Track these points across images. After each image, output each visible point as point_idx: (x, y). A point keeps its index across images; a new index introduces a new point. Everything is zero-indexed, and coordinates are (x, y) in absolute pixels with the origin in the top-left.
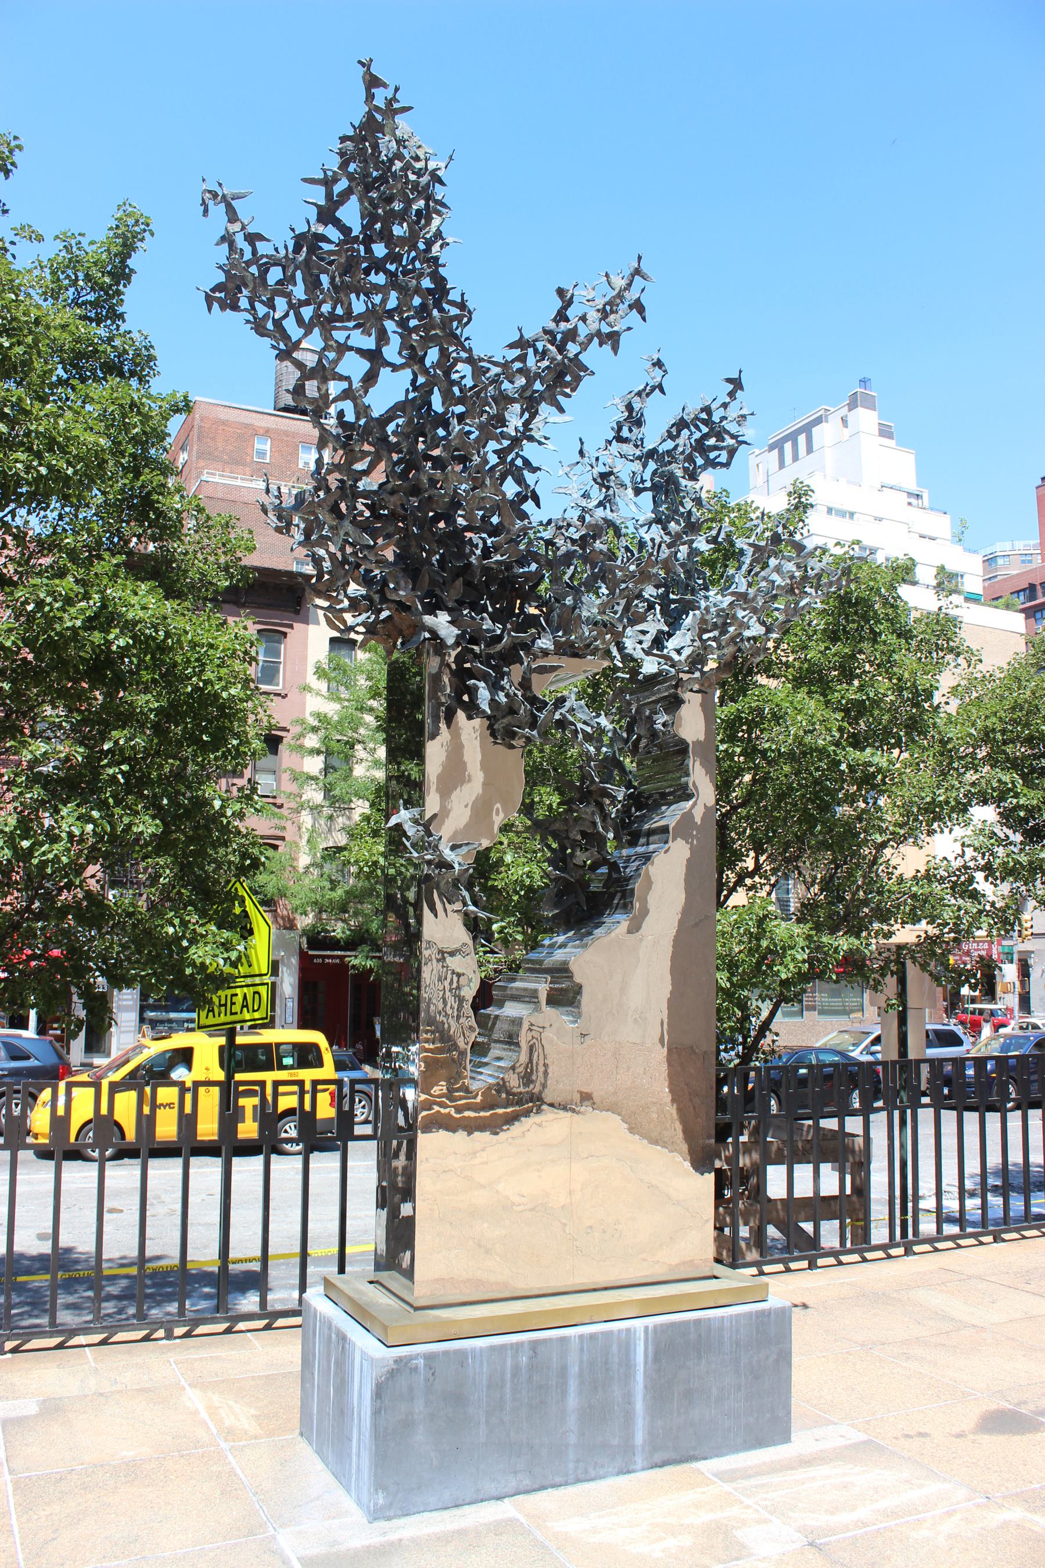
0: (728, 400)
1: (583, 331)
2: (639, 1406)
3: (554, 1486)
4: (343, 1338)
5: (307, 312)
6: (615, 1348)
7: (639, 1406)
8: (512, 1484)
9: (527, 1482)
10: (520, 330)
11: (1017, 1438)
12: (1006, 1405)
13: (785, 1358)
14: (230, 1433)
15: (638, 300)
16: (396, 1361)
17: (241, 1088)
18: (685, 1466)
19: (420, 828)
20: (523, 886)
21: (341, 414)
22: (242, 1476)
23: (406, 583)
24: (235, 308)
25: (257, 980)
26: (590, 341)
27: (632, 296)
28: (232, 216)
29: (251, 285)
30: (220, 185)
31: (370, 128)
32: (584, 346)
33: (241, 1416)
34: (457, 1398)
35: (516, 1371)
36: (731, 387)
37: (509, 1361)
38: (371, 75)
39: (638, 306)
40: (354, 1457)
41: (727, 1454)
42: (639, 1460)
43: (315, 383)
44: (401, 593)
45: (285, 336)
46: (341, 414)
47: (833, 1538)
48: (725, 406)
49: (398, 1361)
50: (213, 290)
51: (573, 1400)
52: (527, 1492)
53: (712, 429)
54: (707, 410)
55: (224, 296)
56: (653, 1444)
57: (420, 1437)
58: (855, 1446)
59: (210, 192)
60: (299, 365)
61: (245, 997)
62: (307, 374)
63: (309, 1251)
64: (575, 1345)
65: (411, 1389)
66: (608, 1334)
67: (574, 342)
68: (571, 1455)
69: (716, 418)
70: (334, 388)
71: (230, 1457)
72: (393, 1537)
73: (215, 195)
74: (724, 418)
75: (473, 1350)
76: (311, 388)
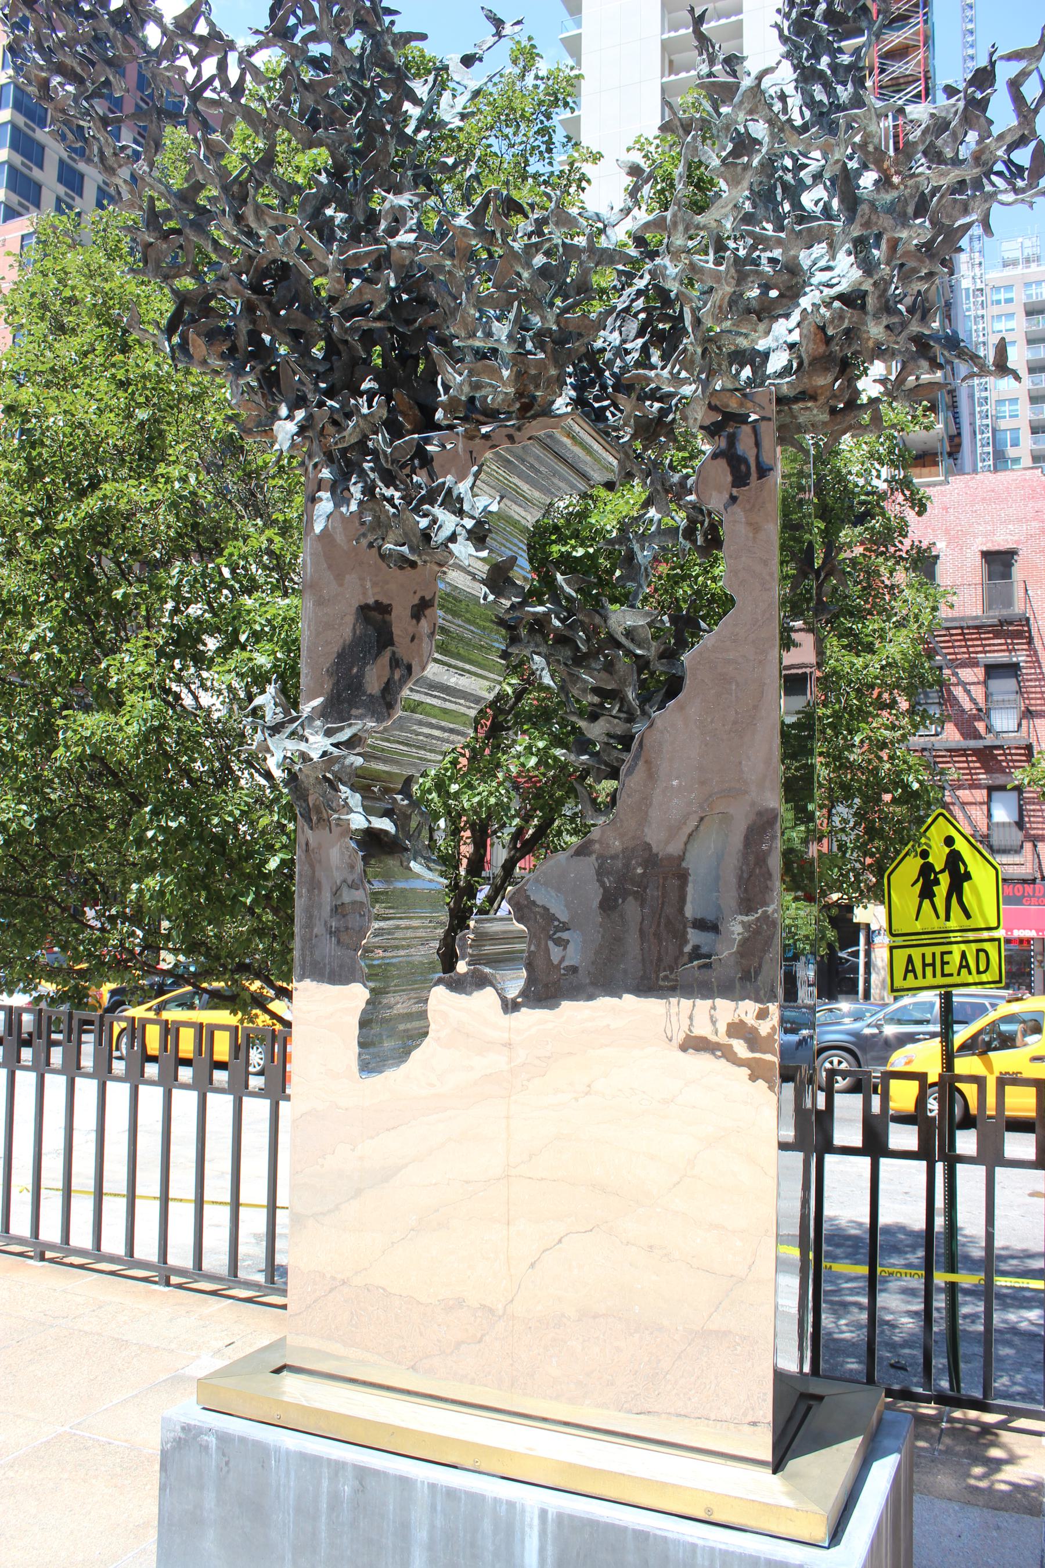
6: (487, 1526)
16: (183, 1428)
21: (687, 476)
25: (986, 935)
35: (335, 1501)
37: (325, 1483)
46: (687, 476)
61: (963, 955)
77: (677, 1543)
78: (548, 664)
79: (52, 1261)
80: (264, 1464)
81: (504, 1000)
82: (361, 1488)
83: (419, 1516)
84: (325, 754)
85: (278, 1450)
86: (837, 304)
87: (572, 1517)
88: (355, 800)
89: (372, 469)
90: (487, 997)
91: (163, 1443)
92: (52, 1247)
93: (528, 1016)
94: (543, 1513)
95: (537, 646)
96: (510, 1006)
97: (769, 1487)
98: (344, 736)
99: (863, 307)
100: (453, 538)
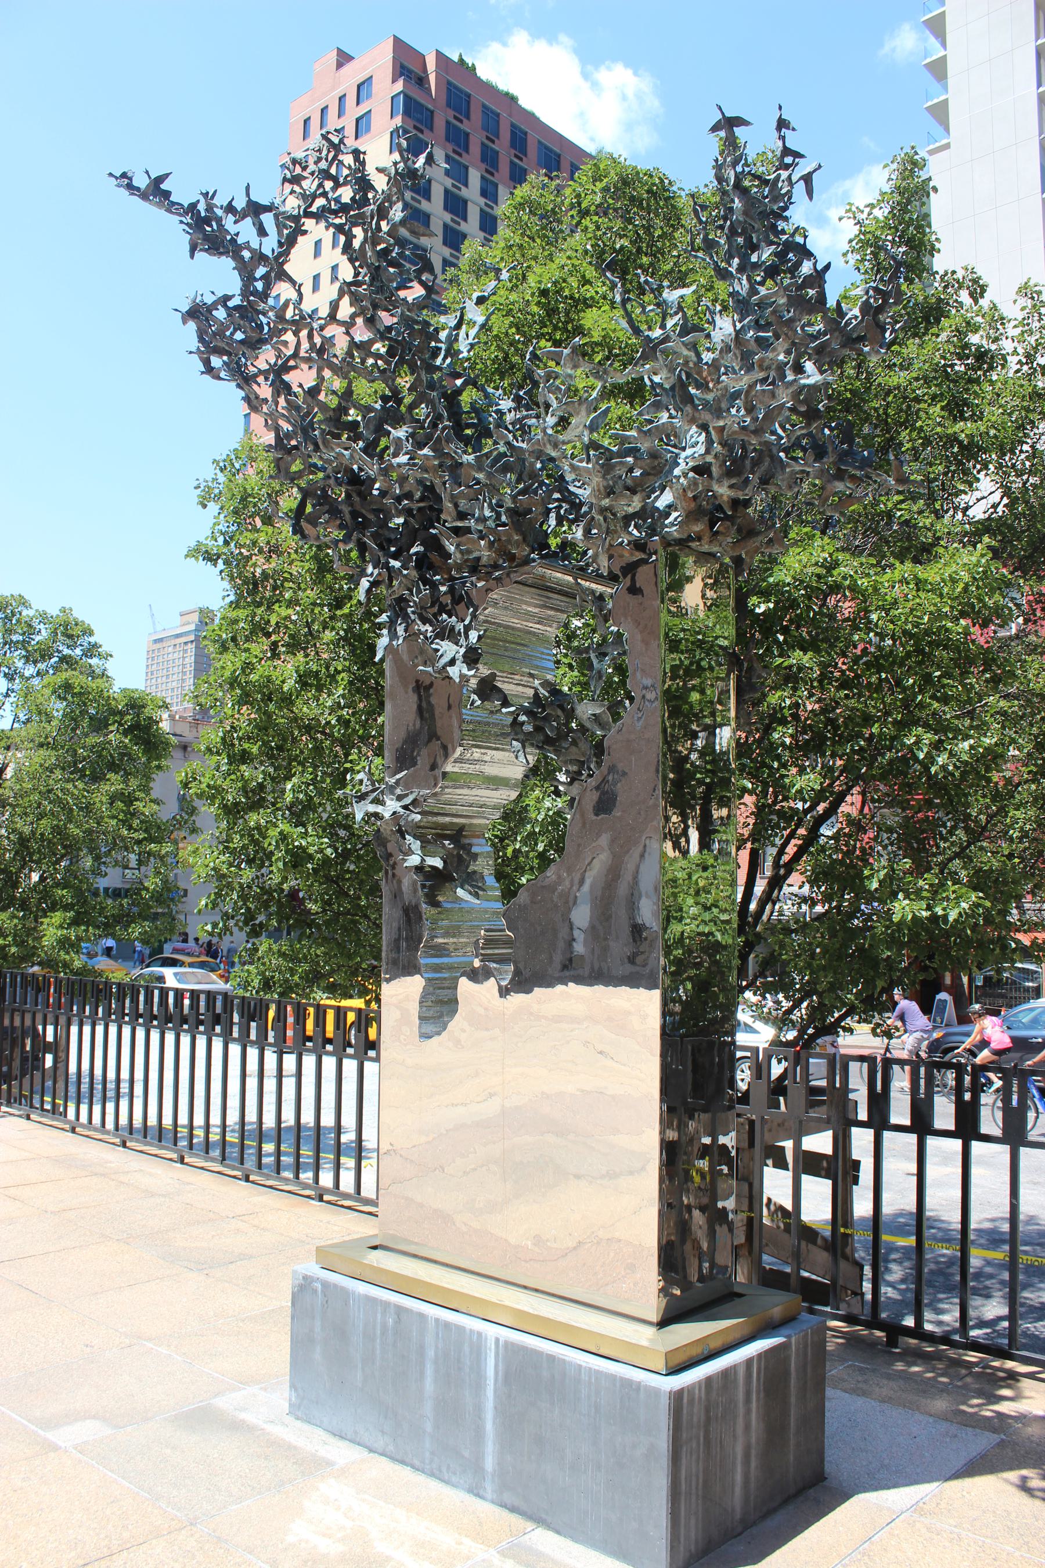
2: (489, 1426)
3: (413, 1467)
6: (466, 1348)
7: (489, 1426)
8: (380, 1443)
37: (379, 1316)
63: (343, 1123)
77: (570, 1363)
78: (524, 747)
79: (329, 1202)
80: (346, 1303)
81: (500, 987)
82: (398, 1321)
83: (430, 1339)
84: (394, 813)
85: (354, 1293)
86: (691, 474)
87: (513, 1344)
88: (416, 845)
89: (413, 613)
90: (491, 985)
91: (293, 1287)
92: (327, 1191)
93: (517, 999)
94: (497, 1340)
95: (516, 734)
96: (504, 992)
97: (645, 1336)
98: (407, 801)
99: (710, 476)
100: (452, 662)
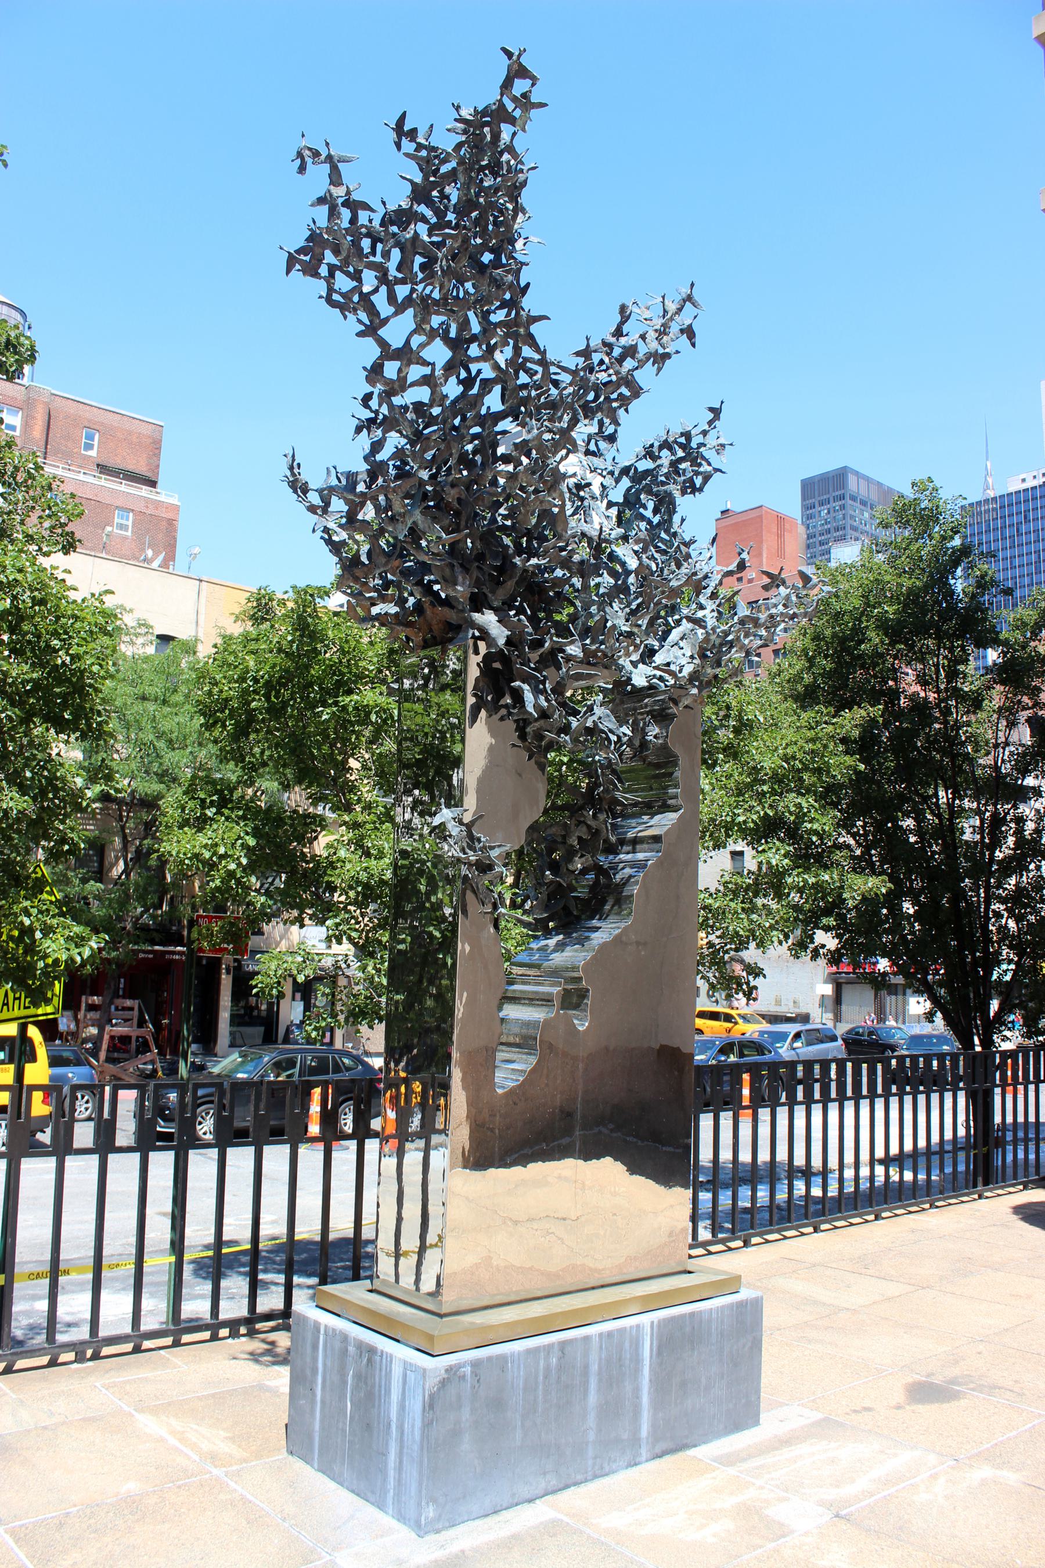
0: (706, 427)
1: (642, 350)
2: (645, 1399)
3: (576, 1484)
4: (372, 1350)
5: (402, 291)
6: (627, 1345)
7: (645, 1399)
9: (554, 1482)
10: (588, 339)
11: (945, 1406)
12: (918, 1378)
13: (757, 1345)
14: (213, 1458)
15: (690, 326)
16: (447, 1371)
17: (200, 1092)
18: (680, 1455)
19: (464, 828)
20: (358, 882)
22: (257, 1502)
23: (464, 579)
24: (316, 275)
26: (648, 359)
27: (685, 318)
28: (336, 178)
29: (344, 254)
30: (327, 144)
31: (497, 115)
32: (641, 364)
33: (214, 1439)
34: (498, 1404)
36: (711, 416)
37: (542, 1362)
38: (520, 65)
39: (689, 332)
40: (391, 1473)
41: (711, 1441)
42: (644, 1452)
43: (397, 364)
44: (459, 588)
45: (372, 310)
47: (852, 1509)
48: (704, 433)
49: (449, 1370)
50: (298, 252)
51: (593, 1398)
52: (554, 1492)
53: (689, 454)
54: (687, 435)
55: (306, 259)
56: (656, 1435)
57: (466, 1445)
58: (817, 1423)
59: (310, 149)
60: (383, 343)
62: (388, 353)
64: (595, 1341)
65: (459, 1397)
66: (622, 1331)
67: (633, 358)
68: (590, 1452)
69: (694, 445)
70: (415, 372)
71: (232, 1484)
72: (455, 1548)
73: (316, 154)
74: (701, 445)
75: (512, 1355)
76: (391, 369)
